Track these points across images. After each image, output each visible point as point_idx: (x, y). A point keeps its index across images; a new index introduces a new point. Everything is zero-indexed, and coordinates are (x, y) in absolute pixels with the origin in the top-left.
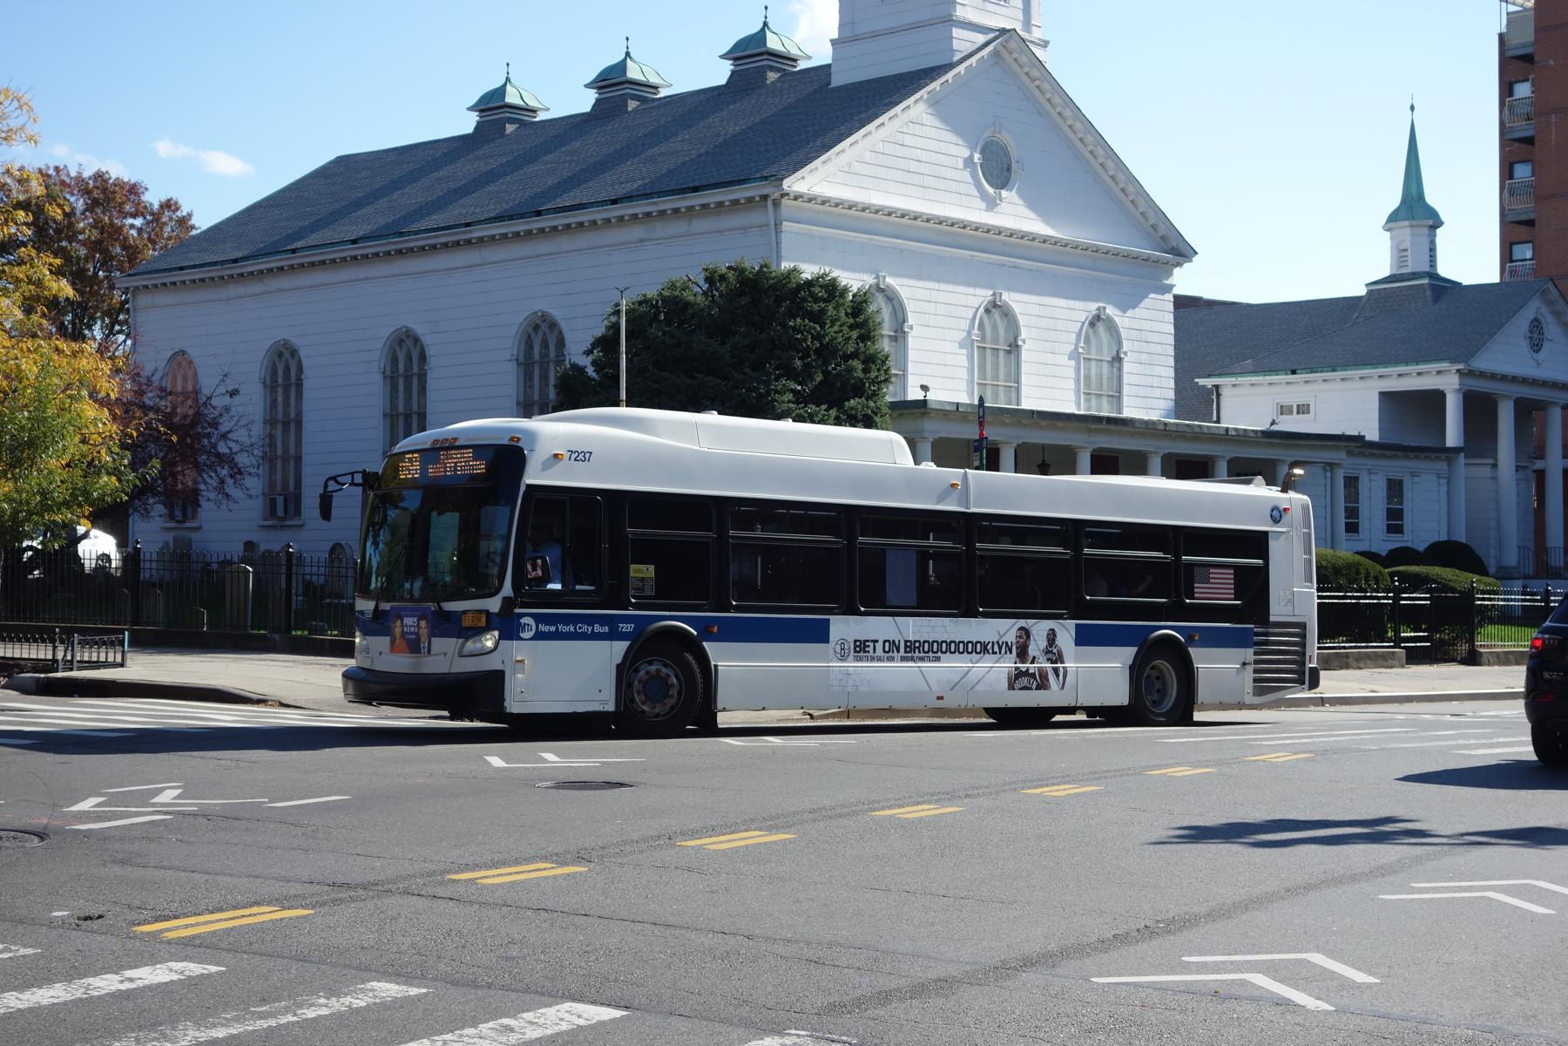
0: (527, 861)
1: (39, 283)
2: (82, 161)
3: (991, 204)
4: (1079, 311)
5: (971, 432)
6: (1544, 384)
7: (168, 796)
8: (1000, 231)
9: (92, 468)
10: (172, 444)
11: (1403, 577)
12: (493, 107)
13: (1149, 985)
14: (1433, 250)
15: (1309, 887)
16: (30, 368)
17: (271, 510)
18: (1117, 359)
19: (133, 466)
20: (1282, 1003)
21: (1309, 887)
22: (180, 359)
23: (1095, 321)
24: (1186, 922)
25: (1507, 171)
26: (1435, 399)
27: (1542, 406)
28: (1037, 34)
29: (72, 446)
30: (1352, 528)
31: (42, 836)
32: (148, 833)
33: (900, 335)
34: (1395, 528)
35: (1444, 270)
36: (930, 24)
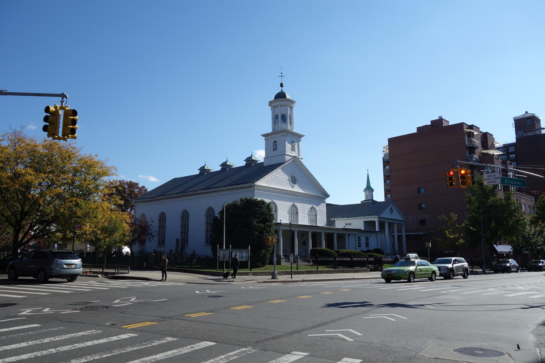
0: (201, 312)
1: (117, 201)
2: (127, 179)
3: (293, 187)
4: (309, 206)
5: (288, 229)
6: (393, 220)
7: (133, 299)
8: (294, 192)
9: (124, 235)
10: (140, 232)
11: (369, 255)
12: (202, 169)
13: (319, 336)
14: (372, 195)
15: (350, 316)
16: (114, 217)
17: (159, 244)
18: (316, 215)
19: (133, 235)
20: (344, 340)
21: (350, 316)
22: (143, 215)
23: (312, 208)
24: (326, 323)
25: (385, 181)
26: (374, 222)
27: (393, 224)
28: (300, 157)
29: (121, 232)
30: (360, 246)
31: (107, 308)
32: (128, 307)
33: (276, 211)
34: (367, 246)
35: (374, 199)
36: (281, 155)
